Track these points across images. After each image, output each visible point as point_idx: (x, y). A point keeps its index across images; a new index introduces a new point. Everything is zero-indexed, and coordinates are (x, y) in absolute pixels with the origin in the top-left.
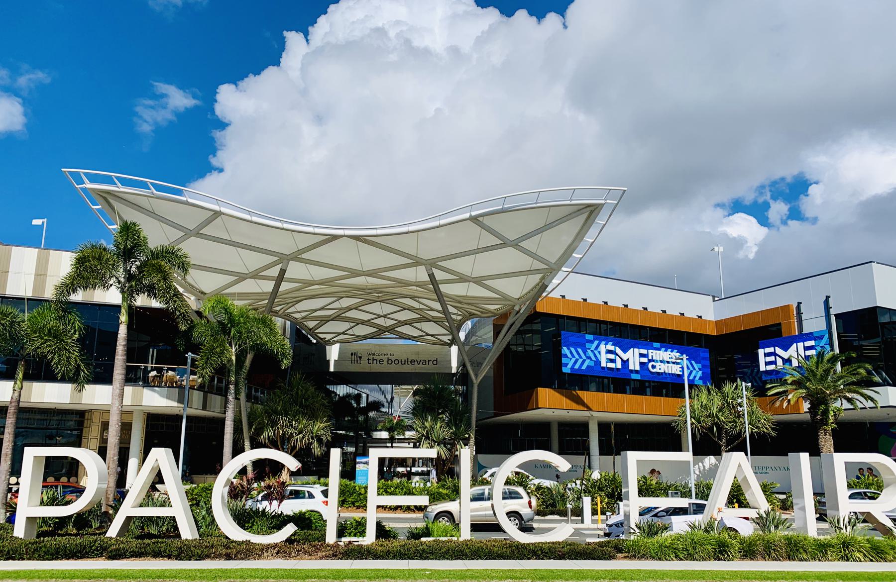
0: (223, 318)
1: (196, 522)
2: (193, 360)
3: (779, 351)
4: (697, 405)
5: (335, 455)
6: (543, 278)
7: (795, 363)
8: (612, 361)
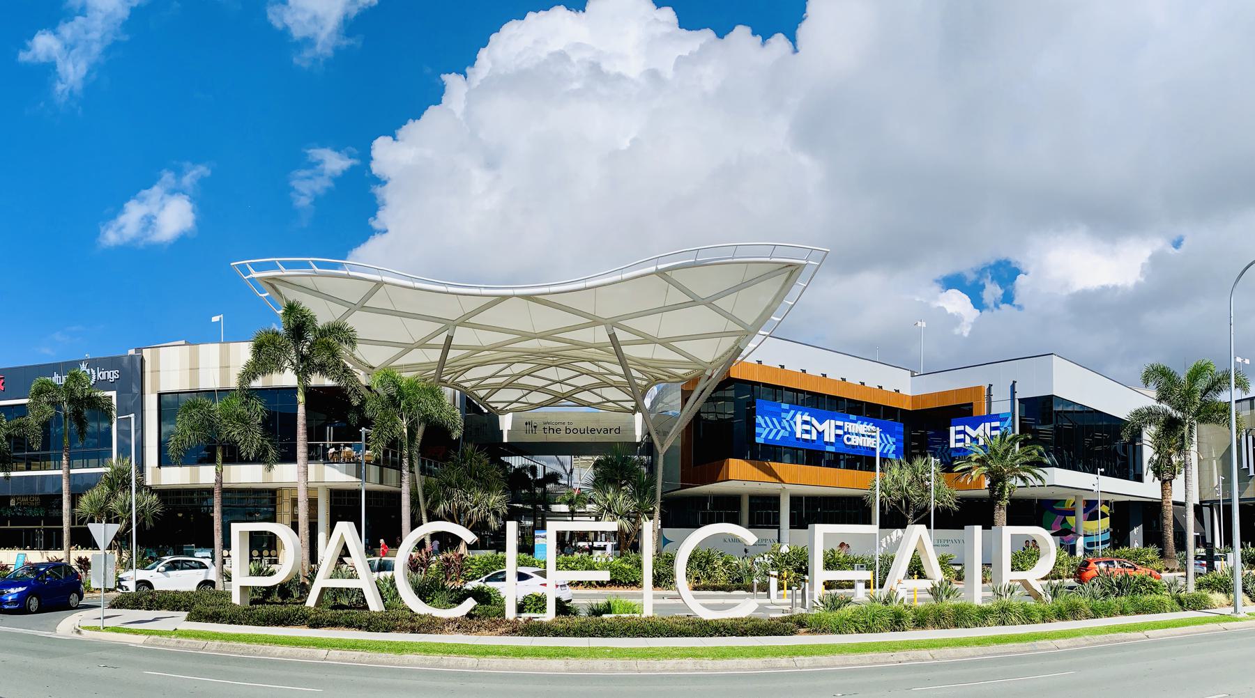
0: (393, 391)
1: (381, 594)
2: (367, 435)
3: (968, 429)
4: (888, 479)
5: (512, 527)
6: (738, 341)
7: (981, 442)
8: (807, 432)
